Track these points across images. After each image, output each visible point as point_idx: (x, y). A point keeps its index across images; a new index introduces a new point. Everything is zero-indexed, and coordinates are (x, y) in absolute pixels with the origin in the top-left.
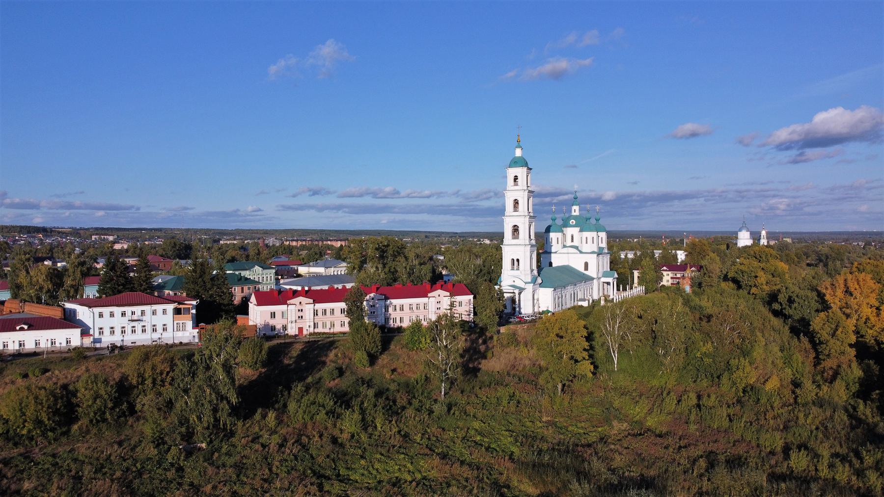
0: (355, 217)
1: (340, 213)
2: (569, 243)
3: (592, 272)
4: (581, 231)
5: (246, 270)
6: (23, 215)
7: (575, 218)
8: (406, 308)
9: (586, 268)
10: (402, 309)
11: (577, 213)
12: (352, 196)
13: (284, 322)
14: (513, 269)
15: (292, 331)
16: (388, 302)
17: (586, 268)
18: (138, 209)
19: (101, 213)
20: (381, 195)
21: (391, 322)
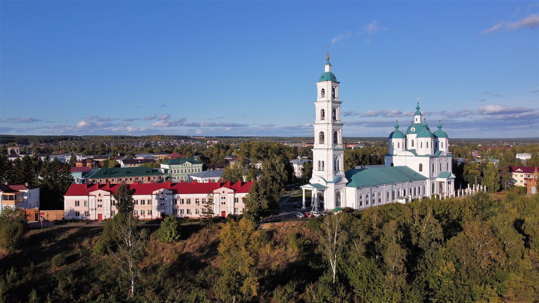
0: (370, 129)
1: (362, 127)
2: (410, 147)
3: (426, 173)
4: (417, 137)
5: (179, 164)
6: (192, 130)
7: (417, 126)
8: (193, 202)
9: (421, 169)
10: (189, 202)
11: (419, 122)
12: (370, 116)
13: (86, 209)
14: (319, 170)
15: (93, 216)
16: (176, 196)
17: (421, 169)
18: (248, 126)
19: (229, 128)
20: (389, 115)
21: (179, 212)
